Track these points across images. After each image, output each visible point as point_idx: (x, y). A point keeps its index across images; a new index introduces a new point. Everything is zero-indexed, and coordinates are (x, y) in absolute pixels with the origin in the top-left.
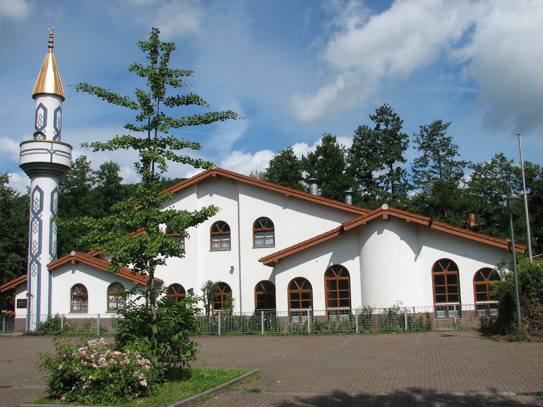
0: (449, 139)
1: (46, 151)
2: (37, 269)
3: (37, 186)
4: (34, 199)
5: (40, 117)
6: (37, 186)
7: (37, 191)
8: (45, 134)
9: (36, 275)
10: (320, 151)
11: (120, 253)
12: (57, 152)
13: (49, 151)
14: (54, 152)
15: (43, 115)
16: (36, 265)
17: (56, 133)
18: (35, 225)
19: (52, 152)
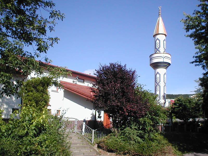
0: (47, 2)
1: (161, 57)
2: (159, 89)
3: (157, 38)
4: (156, 43)
5: (158, 78)
6: (157, 38)
7: (157, 40)
8: (160, 85)
9: (159, 91)
10: (49, 86)
11: (17, 79)
12: (166, 57)
13: (162, 57)
14: (164, 57)
15: (159, 43)
16: (159, 87)
17: (164, 50)
18: (158, 88)
19: (163, 57)
